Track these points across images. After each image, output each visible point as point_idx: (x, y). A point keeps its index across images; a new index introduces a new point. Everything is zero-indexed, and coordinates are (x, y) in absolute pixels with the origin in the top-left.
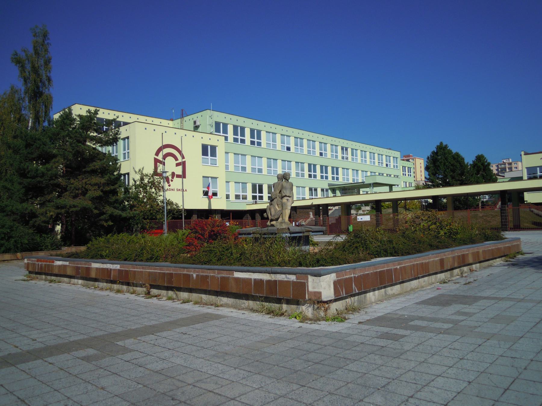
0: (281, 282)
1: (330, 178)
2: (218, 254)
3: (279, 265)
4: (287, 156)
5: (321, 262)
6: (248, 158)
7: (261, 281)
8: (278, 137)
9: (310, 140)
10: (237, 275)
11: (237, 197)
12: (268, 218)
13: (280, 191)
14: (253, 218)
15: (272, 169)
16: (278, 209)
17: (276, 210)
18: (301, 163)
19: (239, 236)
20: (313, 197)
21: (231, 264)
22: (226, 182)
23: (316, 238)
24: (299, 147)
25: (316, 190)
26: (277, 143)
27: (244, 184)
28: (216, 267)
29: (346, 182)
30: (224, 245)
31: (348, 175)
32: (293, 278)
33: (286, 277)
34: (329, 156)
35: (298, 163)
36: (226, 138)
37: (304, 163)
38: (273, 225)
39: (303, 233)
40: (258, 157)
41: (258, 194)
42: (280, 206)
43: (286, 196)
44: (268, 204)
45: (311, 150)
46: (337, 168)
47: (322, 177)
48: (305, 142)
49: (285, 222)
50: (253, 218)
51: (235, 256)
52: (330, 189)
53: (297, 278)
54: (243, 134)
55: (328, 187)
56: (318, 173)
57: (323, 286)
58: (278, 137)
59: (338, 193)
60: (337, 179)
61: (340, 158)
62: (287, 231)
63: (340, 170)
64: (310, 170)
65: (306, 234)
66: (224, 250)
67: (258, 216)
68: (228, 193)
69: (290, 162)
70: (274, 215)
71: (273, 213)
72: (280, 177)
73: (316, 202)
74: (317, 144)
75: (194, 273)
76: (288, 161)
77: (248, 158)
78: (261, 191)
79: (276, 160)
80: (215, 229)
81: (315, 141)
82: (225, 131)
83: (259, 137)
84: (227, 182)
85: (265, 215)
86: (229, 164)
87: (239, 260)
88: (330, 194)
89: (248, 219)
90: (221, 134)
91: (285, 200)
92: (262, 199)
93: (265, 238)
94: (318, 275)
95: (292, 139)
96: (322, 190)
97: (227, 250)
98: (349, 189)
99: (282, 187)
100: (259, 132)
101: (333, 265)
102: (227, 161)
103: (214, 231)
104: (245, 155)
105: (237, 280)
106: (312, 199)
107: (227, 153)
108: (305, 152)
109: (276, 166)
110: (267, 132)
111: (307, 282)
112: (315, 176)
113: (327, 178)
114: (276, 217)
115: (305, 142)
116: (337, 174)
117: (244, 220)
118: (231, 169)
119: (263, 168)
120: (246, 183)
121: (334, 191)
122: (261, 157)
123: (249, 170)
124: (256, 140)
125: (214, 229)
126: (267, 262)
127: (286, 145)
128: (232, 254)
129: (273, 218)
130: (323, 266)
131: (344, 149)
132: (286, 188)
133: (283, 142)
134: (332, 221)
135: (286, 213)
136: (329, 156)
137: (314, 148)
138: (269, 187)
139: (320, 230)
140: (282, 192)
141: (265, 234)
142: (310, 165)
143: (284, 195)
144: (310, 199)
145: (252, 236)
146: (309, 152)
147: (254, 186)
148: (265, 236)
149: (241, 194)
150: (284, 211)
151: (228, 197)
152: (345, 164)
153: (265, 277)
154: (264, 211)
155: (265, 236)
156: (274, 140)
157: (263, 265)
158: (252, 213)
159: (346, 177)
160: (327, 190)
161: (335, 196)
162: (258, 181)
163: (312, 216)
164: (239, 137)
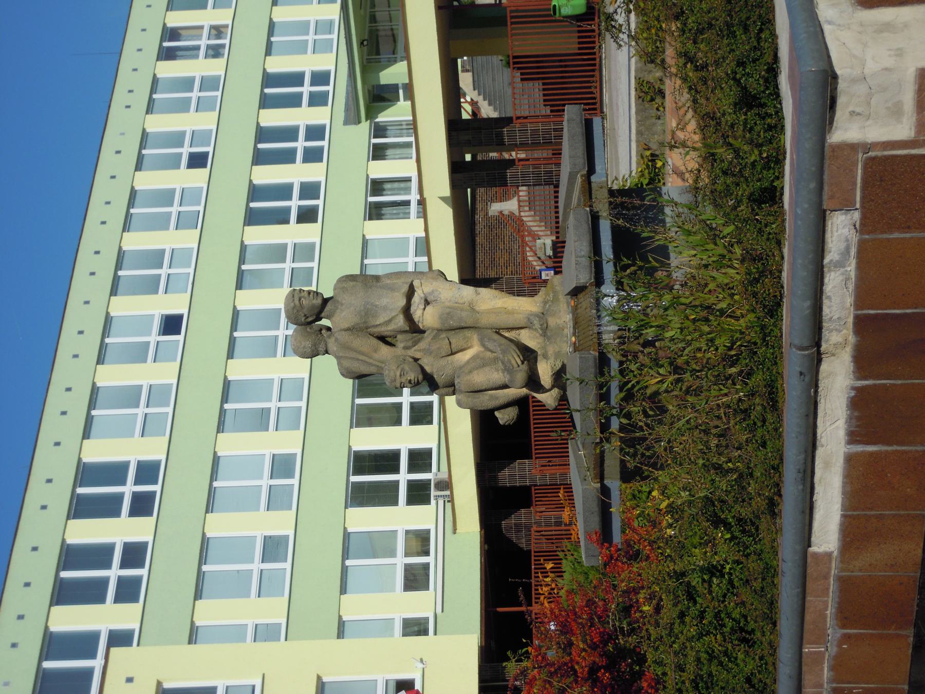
0: (864, 294)
1: (318, 116)
2: (714, 642)
3: (773, 309)
4: (206, 331)
5: (754, 85)
6: (220, 526)
7: (860, 402)
8: (111, 376)
9: (128, 217)
10: (827, 534)
11: (416, 579)
12: (522, 403)
13: (382, 339)
14: (521, 497)
15: (273, 405)
16: (475, 350)
17: (479, 363)
18: (242, 261)
19: (617, 538)
20: (414, 197)
21: (770, 572)
22: (341, 634)
23: (622, 163)
24: (163, 272)
25: (377, 186)
26: (145, 383)
27: (349, 545)
28: (785, 653)
29: (336, 36)
30: (669, 613)
31: (303, 27)
32: (842, 229)
33: (840, 264)
34: (205, 121)
35: (241, 274)
36: (120, 639)
37: (243, 248)
38: (559, 376)
39: (595, 218)
40: (214, 476)
41: (403, 477)
42: (457, 340)
43: (407, 311)
44: (451, 401)
45: (174, 209)
46: (269, 80)
47: (313, 156)
48: (135, 242)
49: (542, 316)
50: (521, 497)
51: (724, 553)
52: (370, 115)
53: (846, 206)
54: (98, 555)
55: (365, 126)
56: (295, 174)
57: (890, 62)
58: (111, 376)
59: (393, 74)
60: (321, 78)
61: (215, 68)
62: (586, 300)
63: (278, 64)
64: (281, 217)
65: (603, 208)
66: (694, 611)
67: (516, 473)
68: (398, 627)
69: (236, 313)
70: (508, 370)
71: (497, 377)
72: (308, 344)
73: (439, 181)
74: (147, 181)
75: (879, 153)
76: (234, 327)
77: (220, 526)
78: (386, 461)
79: (227, 384)
80: (583, 661)
81: (133, 193)
82: (83, 644)
83: (114, 473)
84: (341, 630)
85: (505, 417)
86: (250, 623)
87: (747, 528)
88: (397, 113)
89: (529, 526)
90: (96, 664)
91: (427, 317)
92: (427, 453)
93: (629, 397)
94: (826, 89)
95: (121, 306)
96: (378, 153)
97: (691, 596)
98: (373, 19)
99: (360, 329)
100: (87, 473)
101: (768, 22)
102: (234, 634)
103: (593, 670)
104: (205, 542)
105: (853, 533)
106: (422, 202)
107: (193, 636)
108: (187, 239)
109: (260, 388)
110: (86, 435)
111: (867, 147)
112: (310, 190)
113: (316, 132)
114: (515, 358)
115: (135, 242)
116: (296, 79)
117: (533, 543)
118: (272, 611)
119: (268, 452)
120: (347, 535)
121: (381, 97)
122: (216, 460)
123: (279, 524)
124: (128, 489)
125: (582, 668)
126: (758, 379)
127: (154, 337)
128: (714, 570)
129: (521, 376)
130: (773, 71)
131: (172, 45)
132: (368, 312)
133: (138, 354)
134: (529, 99)
135: (494, 311)
136: (205, 121)
137: (166, 197)
138: (365, 418)
139: (579, 130)
140: (385, 330)
141: (604, 397)
142: (253, 218)
143: (400, 322)
144: (423, 214)
145: (614, 484)
146: (184, 222)
147: (361, 496)
148: (616, 396)
149: (400, 561)
150: (485, 321)
151: (416, 627)
152: (247, 42)
153: (838, 379)
154: (484, 422)
155: (616, 396)
156: (130, 397)
157: (773, 400)
158: (496, 502)
159: (311, 37)
160: (379, 131)
161: (409, 90)
162: (331, 476)
163: (510, 206)
164: (114, 573)
